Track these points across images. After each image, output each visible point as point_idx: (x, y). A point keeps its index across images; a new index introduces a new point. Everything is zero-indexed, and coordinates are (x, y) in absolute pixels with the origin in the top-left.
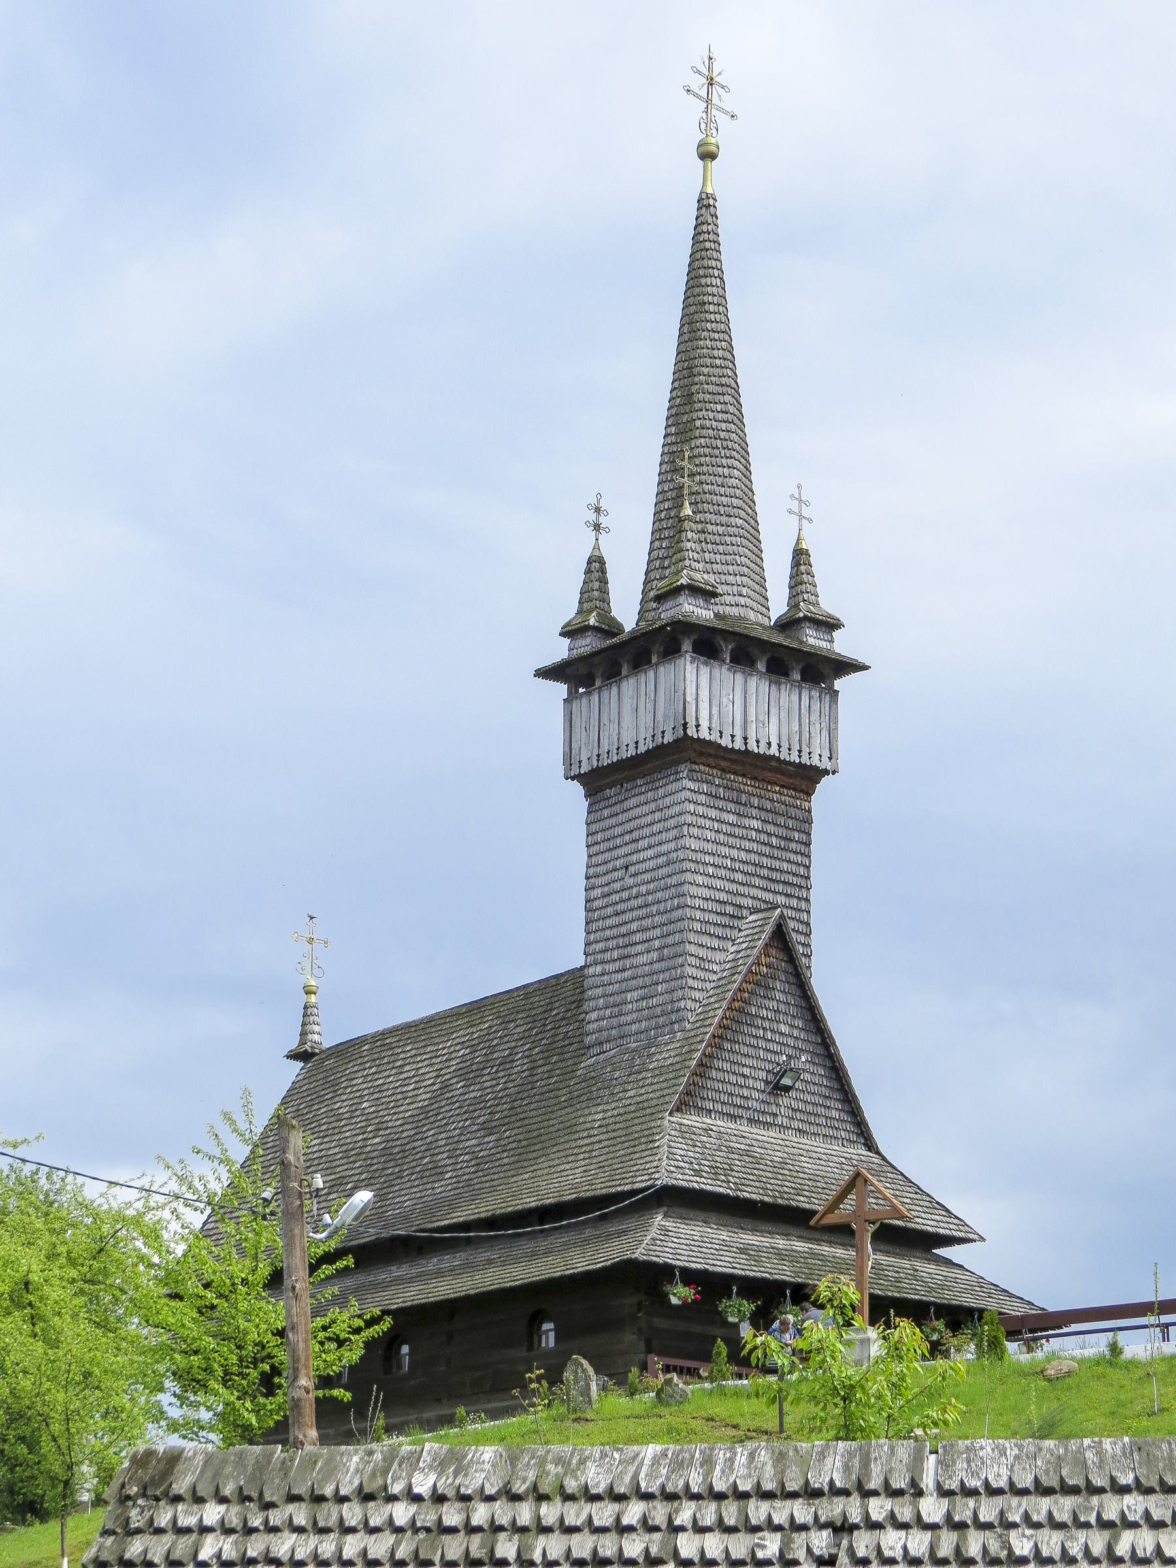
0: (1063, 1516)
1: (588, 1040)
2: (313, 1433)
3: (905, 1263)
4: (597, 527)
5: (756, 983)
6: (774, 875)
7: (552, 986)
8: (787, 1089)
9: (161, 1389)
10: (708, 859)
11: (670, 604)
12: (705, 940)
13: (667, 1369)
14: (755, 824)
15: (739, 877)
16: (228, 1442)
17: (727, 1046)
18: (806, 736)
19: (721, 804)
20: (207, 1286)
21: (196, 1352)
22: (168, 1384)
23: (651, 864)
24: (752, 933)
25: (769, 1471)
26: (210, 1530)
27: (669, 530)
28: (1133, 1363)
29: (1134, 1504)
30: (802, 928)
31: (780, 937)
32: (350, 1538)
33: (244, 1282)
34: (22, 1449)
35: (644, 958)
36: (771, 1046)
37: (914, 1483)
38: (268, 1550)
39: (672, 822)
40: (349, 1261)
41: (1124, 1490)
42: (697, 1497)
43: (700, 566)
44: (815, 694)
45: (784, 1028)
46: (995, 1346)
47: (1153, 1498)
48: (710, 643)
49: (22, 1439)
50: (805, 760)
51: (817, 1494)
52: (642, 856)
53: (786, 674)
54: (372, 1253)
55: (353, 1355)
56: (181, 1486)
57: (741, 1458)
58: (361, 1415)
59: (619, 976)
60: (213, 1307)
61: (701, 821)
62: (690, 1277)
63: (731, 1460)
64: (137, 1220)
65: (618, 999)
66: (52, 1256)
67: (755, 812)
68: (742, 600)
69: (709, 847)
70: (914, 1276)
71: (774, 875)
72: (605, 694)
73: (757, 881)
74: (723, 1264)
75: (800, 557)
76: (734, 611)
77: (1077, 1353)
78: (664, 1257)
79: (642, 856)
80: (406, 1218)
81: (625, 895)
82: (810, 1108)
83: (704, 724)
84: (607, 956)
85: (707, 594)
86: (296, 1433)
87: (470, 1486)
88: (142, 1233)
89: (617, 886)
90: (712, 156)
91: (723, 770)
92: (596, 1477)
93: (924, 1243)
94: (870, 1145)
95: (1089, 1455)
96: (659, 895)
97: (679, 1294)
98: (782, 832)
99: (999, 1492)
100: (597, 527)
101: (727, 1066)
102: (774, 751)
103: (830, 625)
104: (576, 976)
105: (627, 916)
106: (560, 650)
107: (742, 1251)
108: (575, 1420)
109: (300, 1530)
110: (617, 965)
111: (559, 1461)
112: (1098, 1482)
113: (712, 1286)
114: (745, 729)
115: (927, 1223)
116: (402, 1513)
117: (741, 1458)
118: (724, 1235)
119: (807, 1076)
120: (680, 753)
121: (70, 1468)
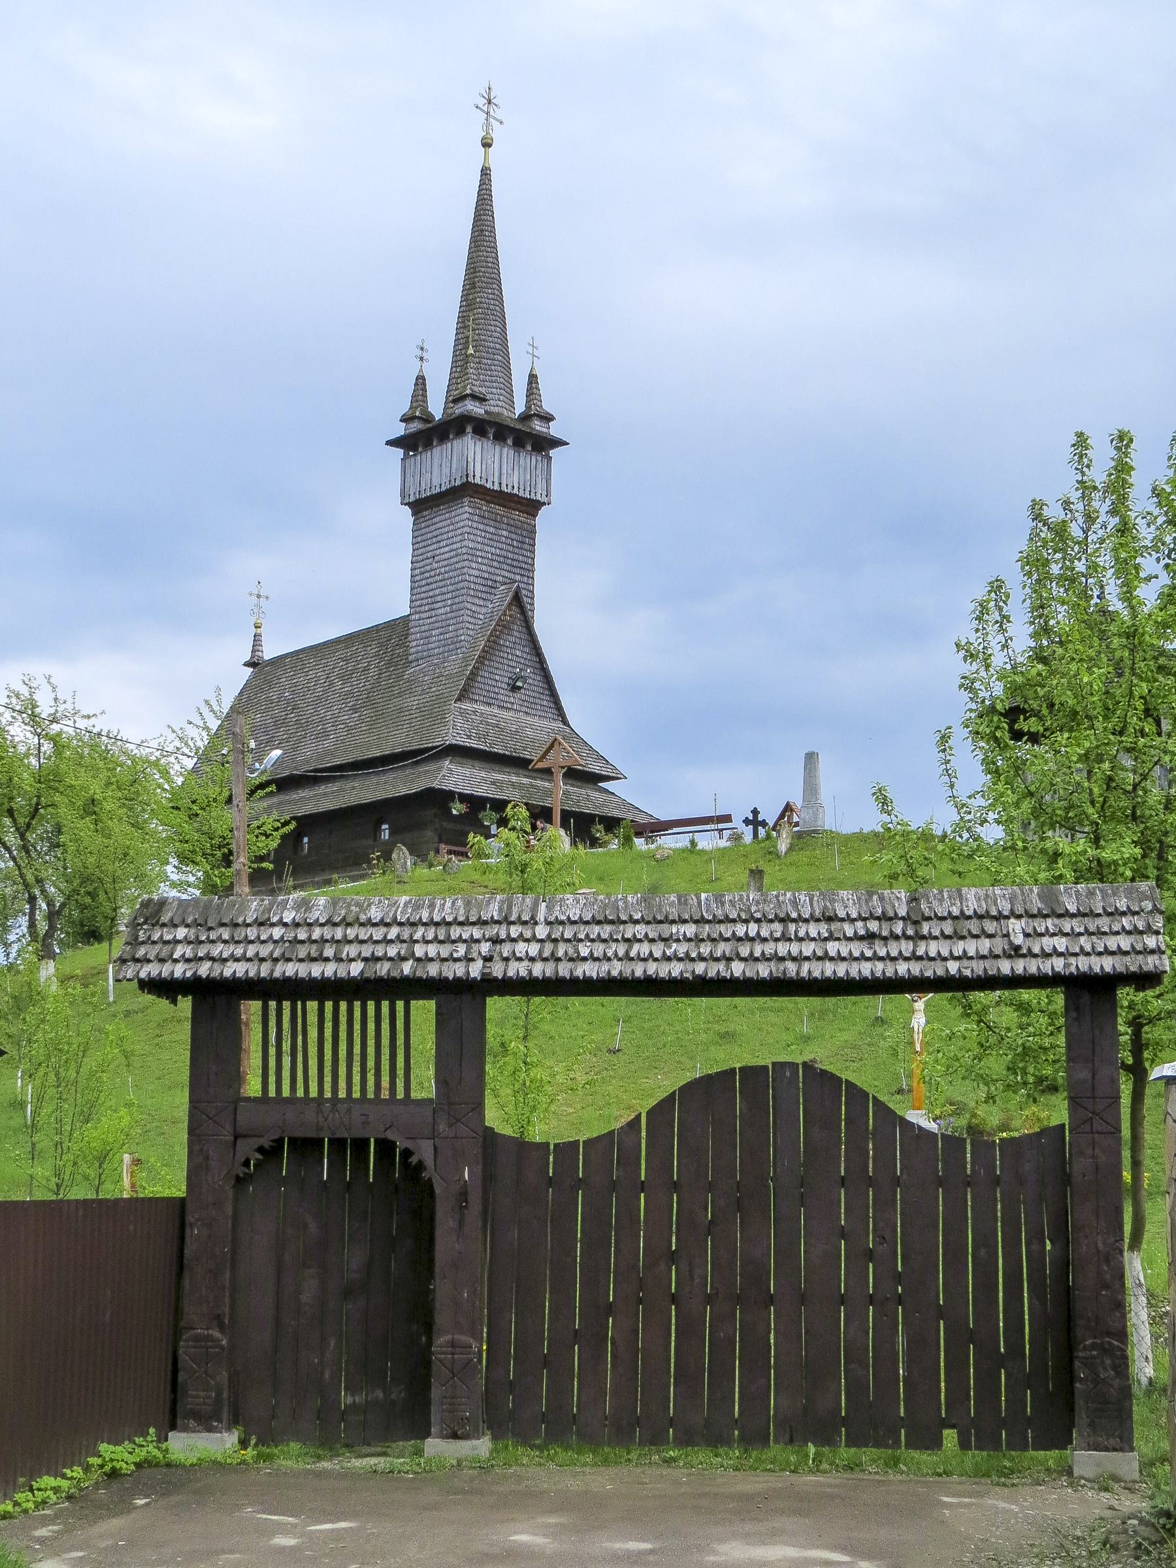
0: (605, 936)
1: (411, 658)
2: (247, 890)
3: (583, 791)
4: (421, 359)
5: (503, 626)
6: (515, 563)
7: (391, 625)
8: (520, 688)
9: (168, 863)
10: (479, 553)
11: (460, 405)
12: (476, 601)
13: (450, 852)
14: (504, 533)
15: (495, 564)
16: (203, 893)
17: (487, 663)
18: (533, 482)
19: (486, 521)
20: (194, 802)
21: (187, 842)
22: (171, 860)
23: (447, 556)
24: (503, 595)
25: (462, 911)
26: (179, 942)
27: (461, 361)
28: (703, 851)
29: (641, 930)
30: (529, 594)
31: (517, 599)
32: (251, 946)
33: (215, 800)
34: (88, 900)
35: (442, 611)
36: (511, 663)
37: (533, 918)
38: (209, 952)
39: (459, 531)
40: (273, 788)
41: (637, 922)
42: (425, 924)
43: (477, 383)
44: (539, 458)
45: (518, 653)
46: (627, 841)
47: (650, 926)
48: (482, 427)
49: (89, 893)
50: (533, 497)
51: (485, 923)
52: (442, 550)
53: (523, 447)
54: (286, 783)
55: (274, 844)
56: (165, 918)
57: (448, 904)
58: (280, 879)
59: (428, 621)
60: (197, 815)
61: (475, 531)
62: (464, 798)
63: (444, 905)
64: (156, 764)
65: (427, 634)
66: (108, 784)
67: (504, 526)
68: (500, 403)
69: (479, 546)
70: (587, 800)
71: (515, 563)
72: (424, 455)
73: (505, 567)
74: (480, 792)
75: (533, 378)
76: (496, 410)
77: (672, 846)
78: (448, 785)
79: (442, 550)
80: (307, 762)
81: (432, 573)
82: (532, 700)
83: (478, 475)
84: (422, 609)
85: (482, 400)
86: (237, 889)
87: (312, 917)
88: (159, 771)
89: (428, 568)
90: (490, 145)
91: (487, 501)
92: (375, 914)
93: (592, 779)
94: (565, 722)
95: (620, 903)
96: (451, 574)
97: (457, 809)
98: (521, 539)
99: (575, 922)
100: (421, 359)
101: (486, 674)
102: (515, 491)
103: (548, 418)
104: (405, 620)
105: (434, 586)
106: (400, 430)
107: (493, 783)
108: (399, 882)
109: (225, 942)
110: (428, 614)
111: (358, 905)
112: (624, 918)
113: (476, 803)
114: (500, 478)
115: (595, 768)
116: (277, 933)
117: (448, 904)
118: (483, 774)
119: (531, 681)
120: (464, 490)
121: (115, 910)
